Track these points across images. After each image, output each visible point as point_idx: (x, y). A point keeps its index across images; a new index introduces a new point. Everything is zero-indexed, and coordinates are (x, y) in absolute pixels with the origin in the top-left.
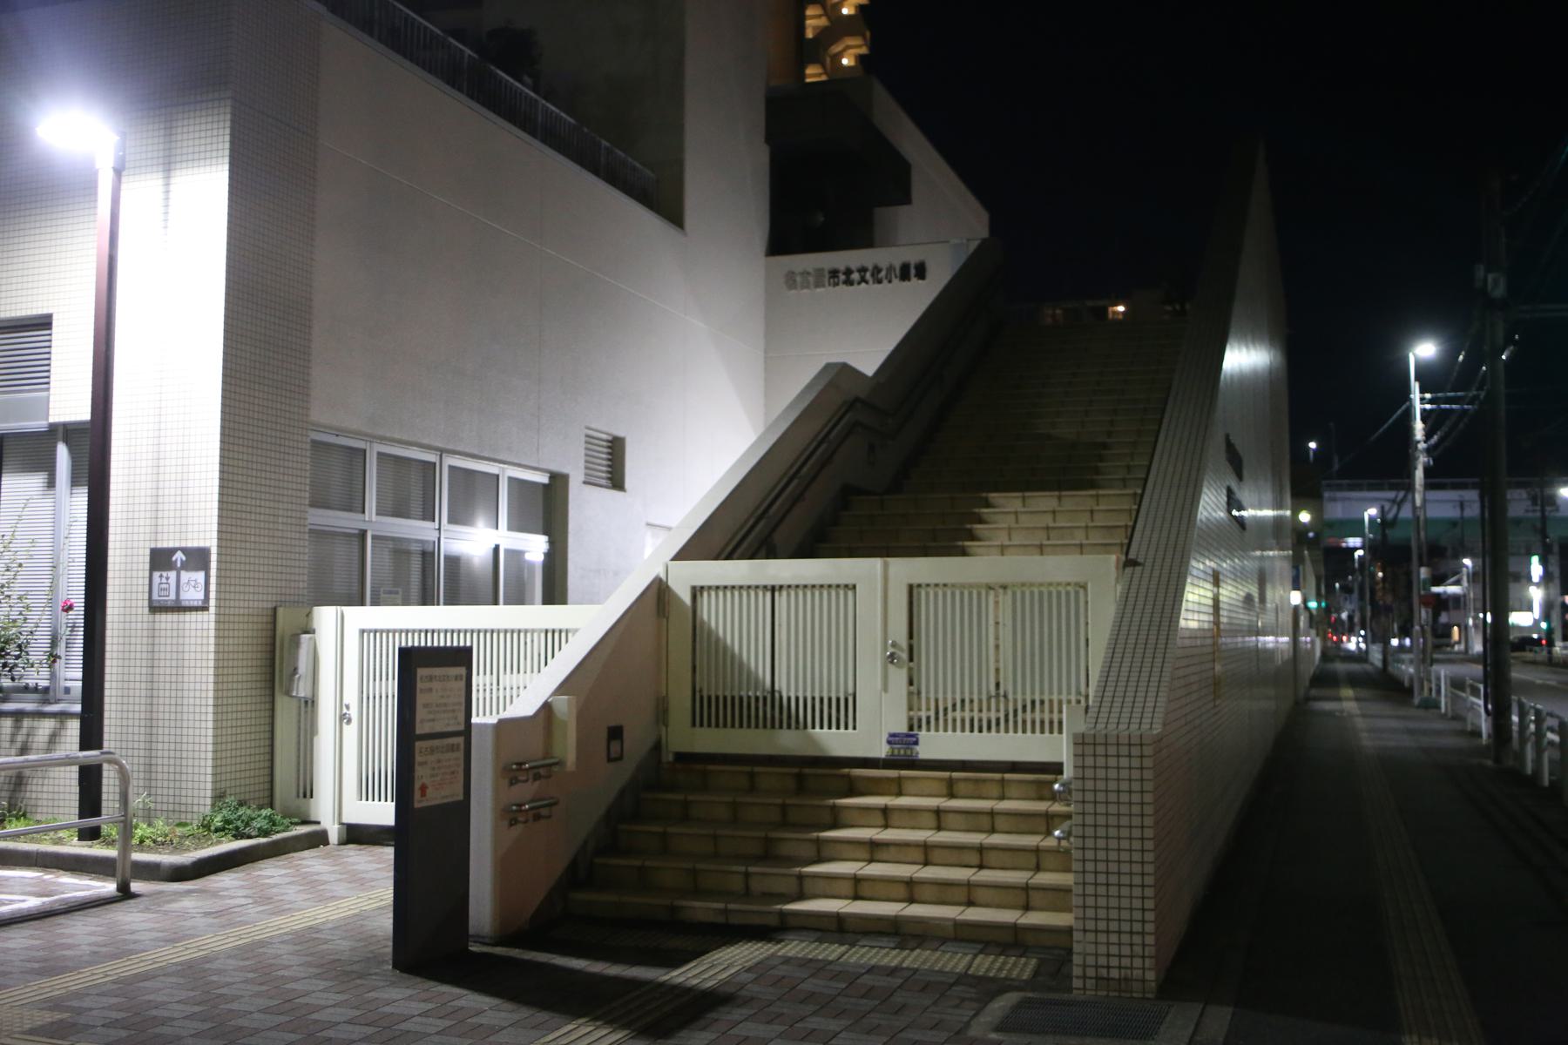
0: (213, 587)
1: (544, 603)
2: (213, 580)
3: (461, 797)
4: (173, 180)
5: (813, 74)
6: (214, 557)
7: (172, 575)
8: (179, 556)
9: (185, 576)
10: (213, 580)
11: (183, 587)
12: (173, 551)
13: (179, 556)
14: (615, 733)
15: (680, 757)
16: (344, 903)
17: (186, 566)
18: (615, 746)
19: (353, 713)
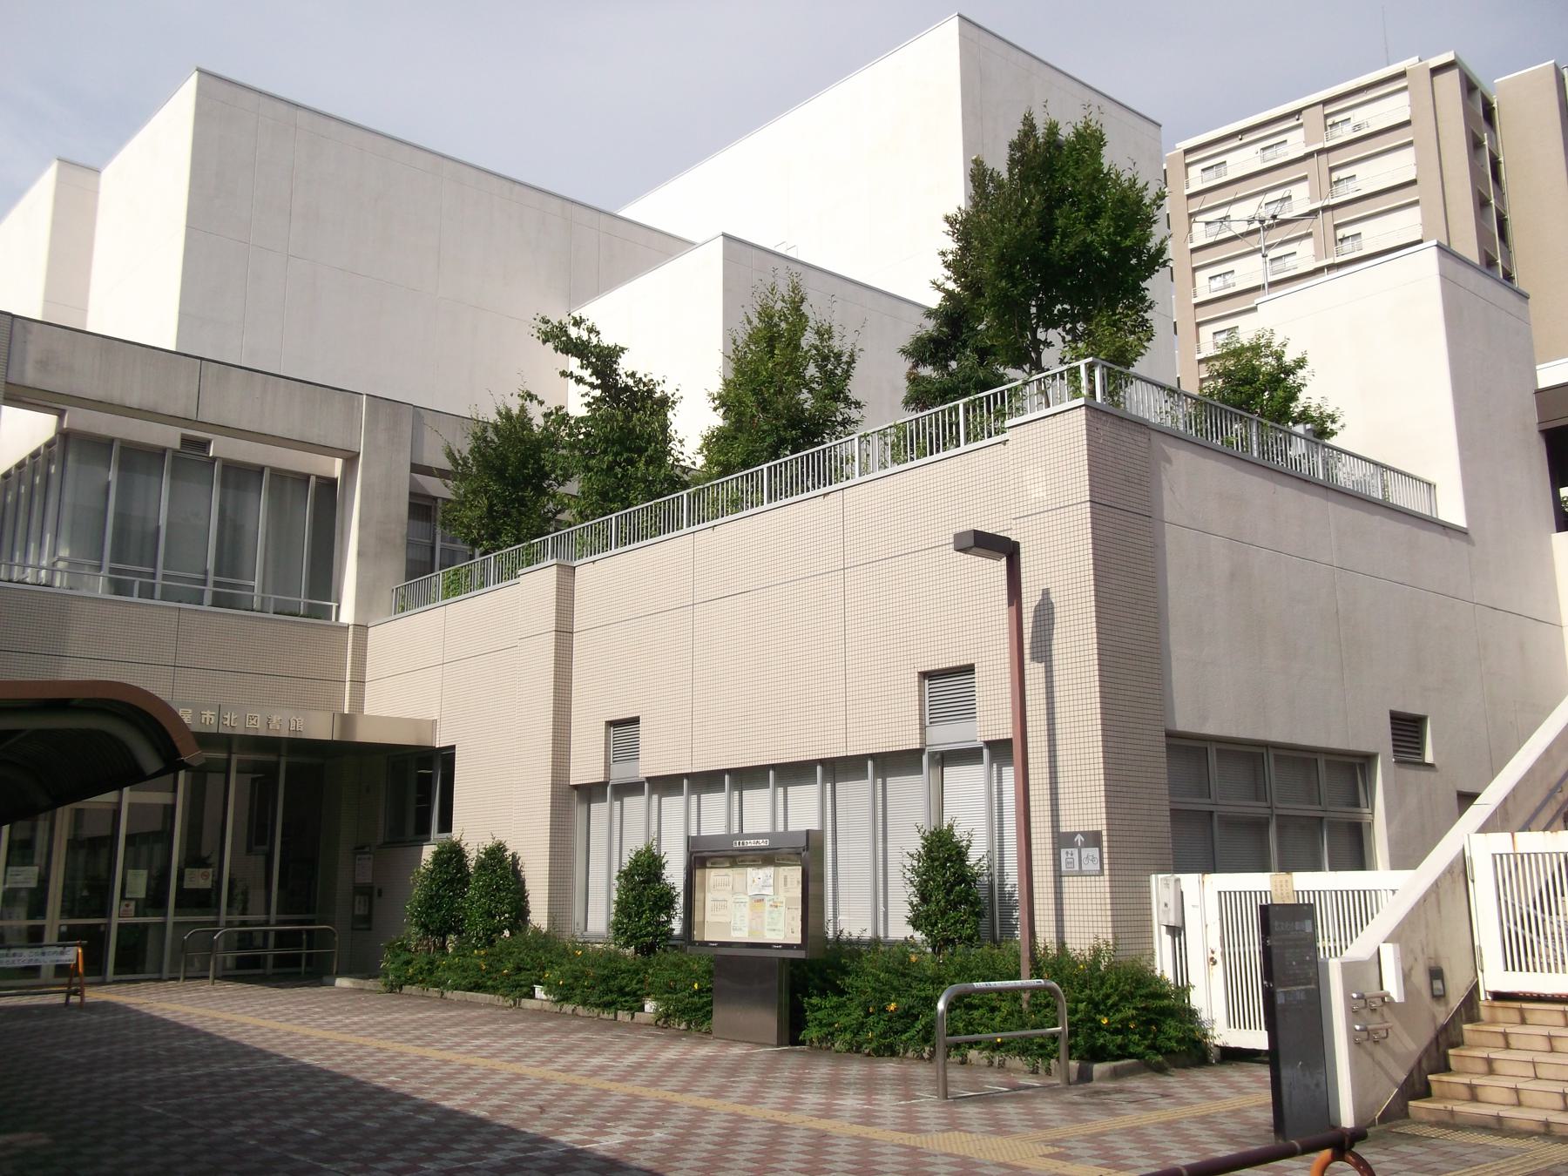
0: (1106, 861)
1: (1393, 868)
2: (1105, 855)
3: (1063, 851)
4: (853, 396)
5: (1068, 326)
6: (1105, 838)
7: (1075, 851)
8: (1079, 838)
9: (1085, 852)
10: (1105, 855)
11: (1084, 861)
12: (1075, 834)
13: (1079, 838)
14: (1436, 974)
15: (1498, 996)
16: (1228, 1102)
17: (1086, 845)
18: (1438, 984)
19: (1218, 957)
